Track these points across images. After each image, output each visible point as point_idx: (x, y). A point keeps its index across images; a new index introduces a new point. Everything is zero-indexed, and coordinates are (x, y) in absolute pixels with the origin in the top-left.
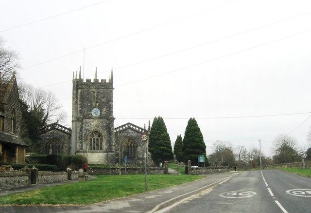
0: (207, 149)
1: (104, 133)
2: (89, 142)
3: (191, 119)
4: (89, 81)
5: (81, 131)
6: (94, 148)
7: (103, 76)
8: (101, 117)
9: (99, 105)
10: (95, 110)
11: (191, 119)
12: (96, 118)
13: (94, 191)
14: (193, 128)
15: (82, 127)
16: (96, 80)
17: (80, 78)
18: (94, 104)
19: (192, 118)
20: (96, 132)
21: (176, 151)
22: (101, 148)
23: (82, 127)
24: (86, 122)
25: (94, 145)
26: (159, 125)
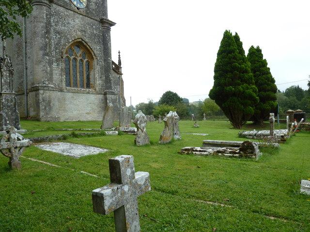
1: (96, 49)
2: (63, 65)
5: (48, 32)
11: (227, 35)
14: (236, 34)
20: (79, 44)
21: (222, 81)
24: (57, 13)
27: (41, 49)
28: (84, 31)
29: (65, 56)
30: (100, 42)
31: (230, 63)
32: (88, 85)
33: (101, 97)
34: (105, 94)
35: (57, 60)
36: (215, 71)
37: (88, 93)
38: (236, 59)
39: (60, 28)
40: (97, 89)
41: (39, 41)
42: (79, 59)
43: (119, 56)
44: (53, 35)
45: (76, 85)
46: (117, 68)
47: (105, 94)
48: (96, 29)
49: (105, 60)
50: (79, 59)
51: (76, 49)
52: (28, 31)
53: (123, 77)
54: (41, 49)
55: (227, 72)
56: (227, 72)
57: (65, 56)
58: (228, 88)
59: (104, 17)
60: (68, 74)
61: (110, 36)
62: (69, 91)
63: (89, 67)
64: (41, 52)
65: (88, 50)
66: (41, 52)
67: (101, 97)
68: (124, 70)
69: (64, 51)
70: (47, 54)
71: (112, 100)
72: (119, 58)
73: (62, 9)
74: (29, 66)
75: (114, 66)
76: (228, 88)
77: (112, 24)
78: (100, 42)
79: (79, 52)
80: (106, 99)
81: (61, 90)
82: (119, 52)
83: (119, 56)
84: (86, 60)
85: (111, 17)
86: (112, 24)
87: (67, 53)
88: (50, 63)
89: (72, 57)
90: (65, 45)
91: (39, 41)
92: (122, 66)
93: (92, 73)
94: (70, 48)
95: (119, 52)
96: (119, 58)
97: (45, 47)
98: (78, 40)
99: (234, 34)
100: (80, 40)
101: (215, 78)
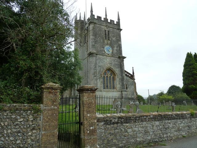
0: (177, 85)
1: (117, 71)
2: (102, 80)
3: (188, 53)
4: (99, 18)
5: (95, 67)
6: (107, 86)
7: (112, 17)
8: (113, 55)
9: (110, 43)
10: (107, 47)
11: (188, 53)
12: (108, 55)
13: (125, 129)
14: (195, 53)
15: (96, 64)
16: (106, 19)
17: (92, 15)
18: (106, 41)
19: (190, 52)
20: (109, 69)
21: (187, 82)
22: (114, 88)
23: (96, 64)
24: (99, 58)
25: (107, 84)
26: (117, 22)
27: (93, 74)
28: (111, 64)
29: (102, 76)
30: (119, 67)
31: (191, 71)
32: (114, 88)
33: (120, 93)
34: (122, 92)
35: (99, 78)
36: (183, 76)
37: (113, 91)
38: (195, 69)
39: (101, 64)
40: (117, 89)
41: (92, 71)
42: (109, 76)
43: (133, 70)
44: (98, 68)
45: (107, 88)
46: (132, 77)
47: (122, 92)
48: (116, 61)
49: (121, 75)
50: (109, 76)
51: (107, 72)
52: (89, 67)
53: (136, 81)
54: (93, 74)
55: (189, 76)
56: (189, 76)
57: (102, 76)
58: (190, 86)
59: (120, 55)
60: (104, 83)
61: (123, 64)
62: (104, 91)
63: (114, 79)
64: (93, 76)
65: (113, 72)
66: (93, 76)
67: (120, 93)
68: (135, 77)
69: (102, 74)
70: (95, 76)
71: (125, 94)
72: (133, 71)
73: (101, 56)
74: (89, 81)
75: (130, 76)
76: (190, 86)
77: (125, 58)
78: (119, 67)
79: (109, 74)
80: (122, 94)
81: (101, 91)
82: (133, 68)
83: (133, 70)
84: (113, 76)
85: (124, 54)
86: (125, 58)
87: (103, 74)
88: (96, 80)
89: (106, 76)
90: (103, 71)
91: (92, 71)
92: (134, 75)
93: (115, 82)
94: (105, 72)
95: (133, 68)
96: (133, 71)
97: (95, 73)
98: (108, 68)
99: (193, 54)
100: (109, 68)
101: (183, 80)
